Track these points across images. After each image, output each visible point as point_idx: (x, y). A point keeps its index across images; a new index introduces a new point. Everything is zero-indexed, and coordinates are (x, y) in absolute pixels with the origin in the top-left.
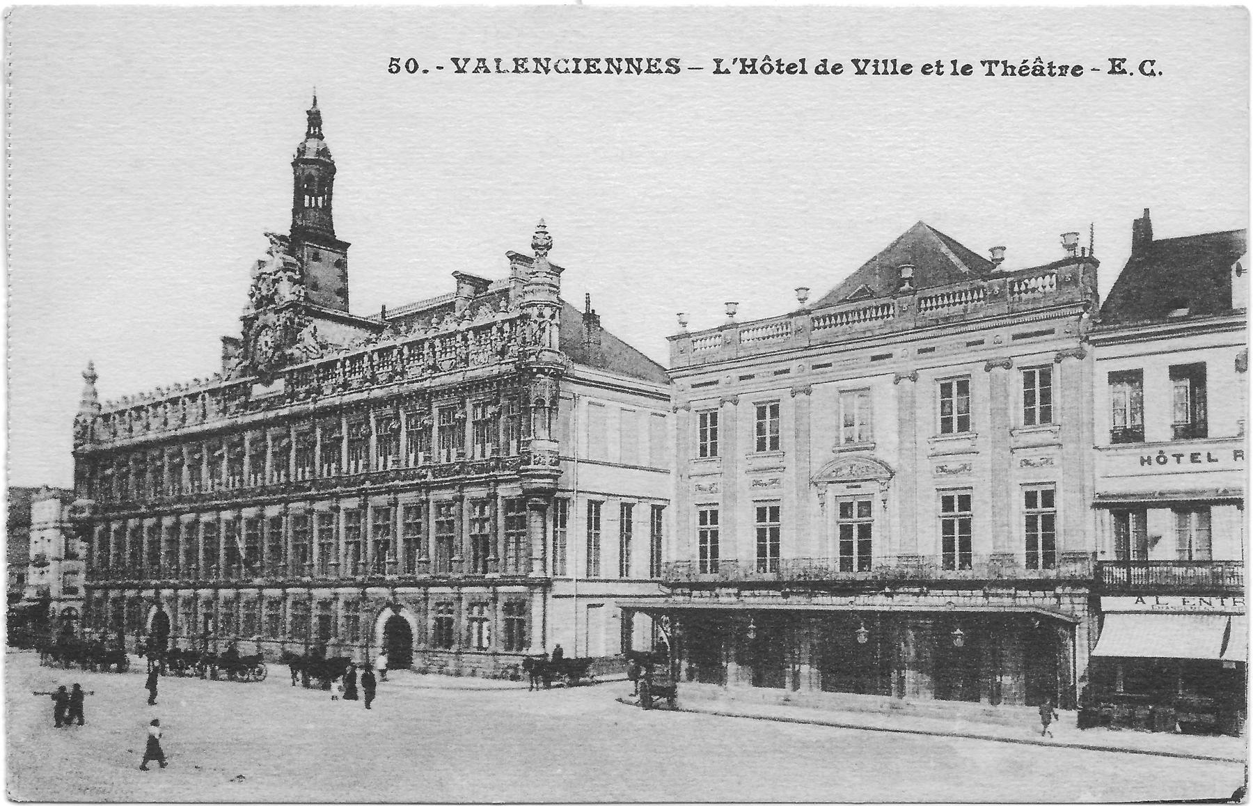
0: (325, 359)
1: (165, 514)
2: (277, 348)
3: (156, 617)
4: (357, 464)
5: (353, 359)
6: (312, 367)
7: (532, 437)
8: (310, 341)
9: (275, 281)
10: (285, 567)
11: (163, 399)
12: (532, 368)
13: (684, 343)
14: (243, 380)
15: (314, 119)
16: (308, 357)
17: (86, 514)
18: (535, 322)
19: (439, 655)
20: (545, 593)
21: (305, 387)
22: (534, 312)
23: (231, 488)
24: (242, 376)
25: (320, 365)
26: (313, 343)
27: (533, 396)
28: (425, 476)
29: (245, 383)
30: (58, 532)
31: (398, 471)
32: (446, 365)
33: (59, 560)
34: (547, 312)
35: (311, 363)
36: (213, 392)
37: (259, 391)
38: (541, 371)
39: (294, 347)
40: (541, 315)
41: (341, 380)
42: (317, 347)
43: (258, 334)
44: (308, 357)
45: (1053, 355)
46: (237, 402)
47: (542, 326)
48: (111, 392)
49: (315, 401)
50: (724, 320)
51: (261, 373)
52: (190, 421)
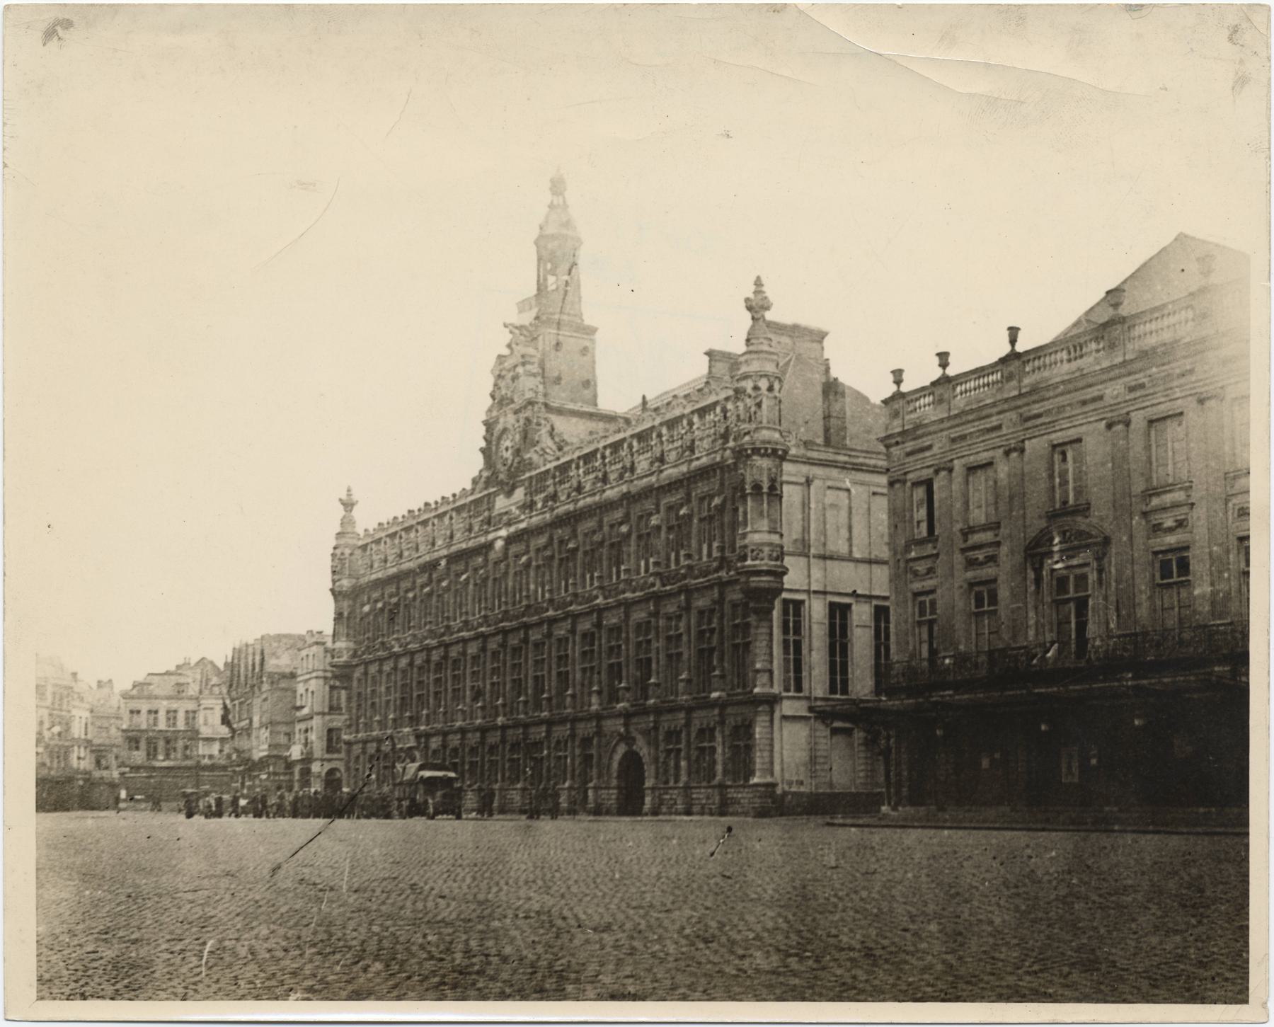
0: (563, 460)
1: (371, 662)
2: (517, 452)
3: (625, 755)
4: (710, 547)
5: (641, 437)
6: (547, 471)
7: (749, 529)
8: (547, 442)
9: (514, 378)
10: (526, 703)
11: (414, 522)
12: (746, 450)
13: (1014, 366)
14: (486, 492)
15: (557, 186)
16: (545, 460)
17: (344, 658)
18: (750, 396)
19: (671, 791)
20: (772, 713)
21: (543, 495)
22: (748, 385)
23: (563, 594)
24: (486, 488)
25: (556, 468)
26: (550, 443)
27: (748, 479)
28: (653, 585)
29: (489, 495)
30: (321, 682)
31: (690, 567)
32: (672, 456)
33: (323, 714)
34: (764, 384)
35: (549, 466)
36: (458, 510)
37: (501, 503)
38: (756, 451)
39: (532, 450)
40: (756, 388)
41: (575, 484)
42: (554, 447)
43: (499, 438)
44: (545, 460)
45: (931, 470)
46: (481, 518)
47: (758, 400)
48: (367, 520)
49: (552, 509)
50: (937, 373)
51: (501, 483)
52: (458, 536)
